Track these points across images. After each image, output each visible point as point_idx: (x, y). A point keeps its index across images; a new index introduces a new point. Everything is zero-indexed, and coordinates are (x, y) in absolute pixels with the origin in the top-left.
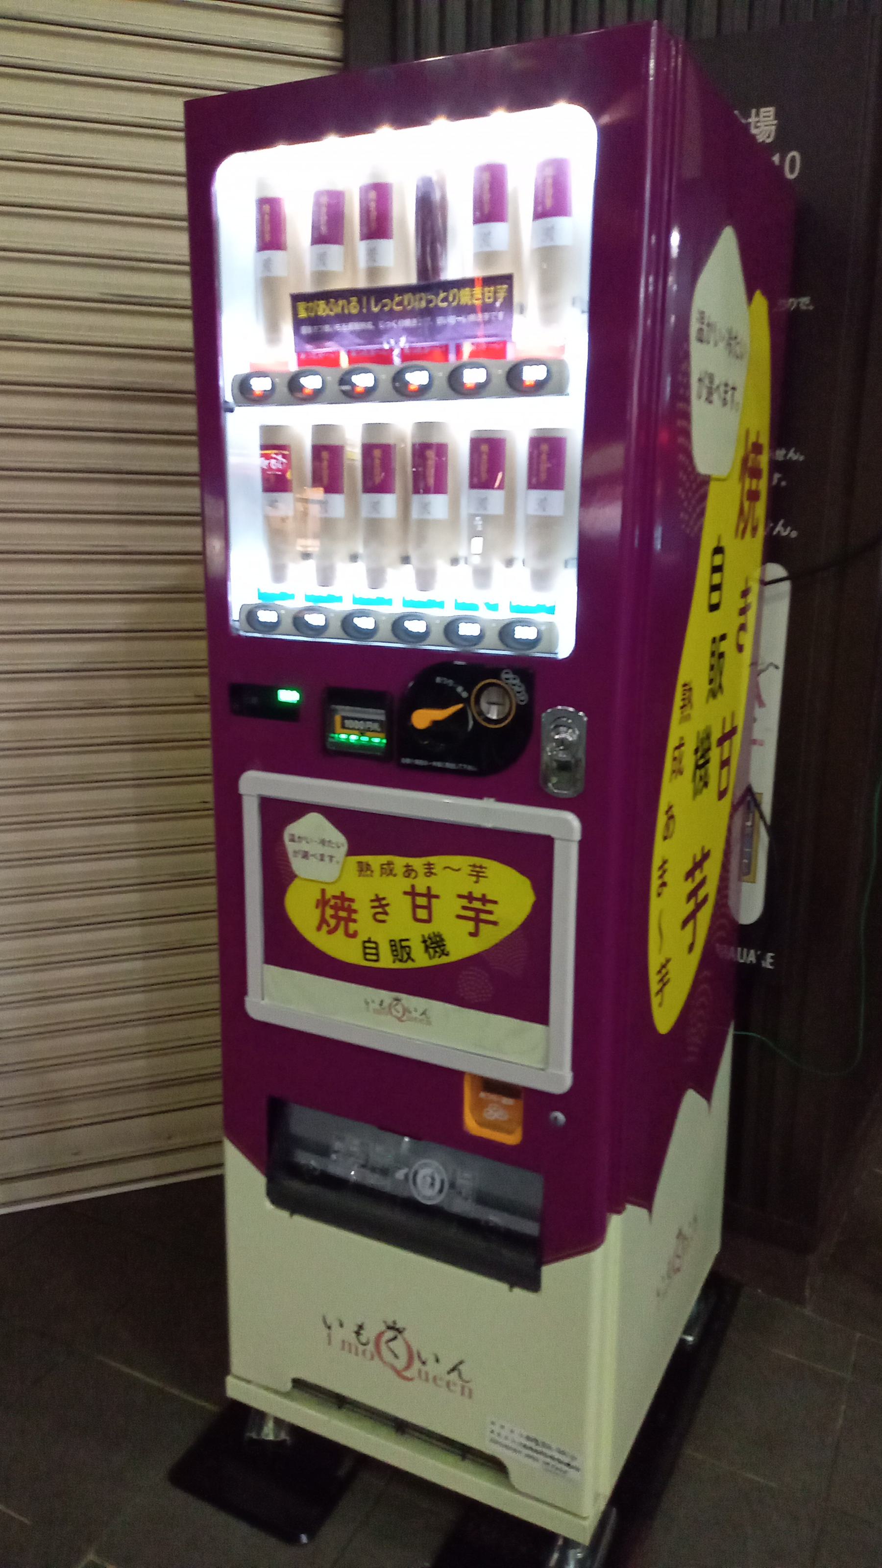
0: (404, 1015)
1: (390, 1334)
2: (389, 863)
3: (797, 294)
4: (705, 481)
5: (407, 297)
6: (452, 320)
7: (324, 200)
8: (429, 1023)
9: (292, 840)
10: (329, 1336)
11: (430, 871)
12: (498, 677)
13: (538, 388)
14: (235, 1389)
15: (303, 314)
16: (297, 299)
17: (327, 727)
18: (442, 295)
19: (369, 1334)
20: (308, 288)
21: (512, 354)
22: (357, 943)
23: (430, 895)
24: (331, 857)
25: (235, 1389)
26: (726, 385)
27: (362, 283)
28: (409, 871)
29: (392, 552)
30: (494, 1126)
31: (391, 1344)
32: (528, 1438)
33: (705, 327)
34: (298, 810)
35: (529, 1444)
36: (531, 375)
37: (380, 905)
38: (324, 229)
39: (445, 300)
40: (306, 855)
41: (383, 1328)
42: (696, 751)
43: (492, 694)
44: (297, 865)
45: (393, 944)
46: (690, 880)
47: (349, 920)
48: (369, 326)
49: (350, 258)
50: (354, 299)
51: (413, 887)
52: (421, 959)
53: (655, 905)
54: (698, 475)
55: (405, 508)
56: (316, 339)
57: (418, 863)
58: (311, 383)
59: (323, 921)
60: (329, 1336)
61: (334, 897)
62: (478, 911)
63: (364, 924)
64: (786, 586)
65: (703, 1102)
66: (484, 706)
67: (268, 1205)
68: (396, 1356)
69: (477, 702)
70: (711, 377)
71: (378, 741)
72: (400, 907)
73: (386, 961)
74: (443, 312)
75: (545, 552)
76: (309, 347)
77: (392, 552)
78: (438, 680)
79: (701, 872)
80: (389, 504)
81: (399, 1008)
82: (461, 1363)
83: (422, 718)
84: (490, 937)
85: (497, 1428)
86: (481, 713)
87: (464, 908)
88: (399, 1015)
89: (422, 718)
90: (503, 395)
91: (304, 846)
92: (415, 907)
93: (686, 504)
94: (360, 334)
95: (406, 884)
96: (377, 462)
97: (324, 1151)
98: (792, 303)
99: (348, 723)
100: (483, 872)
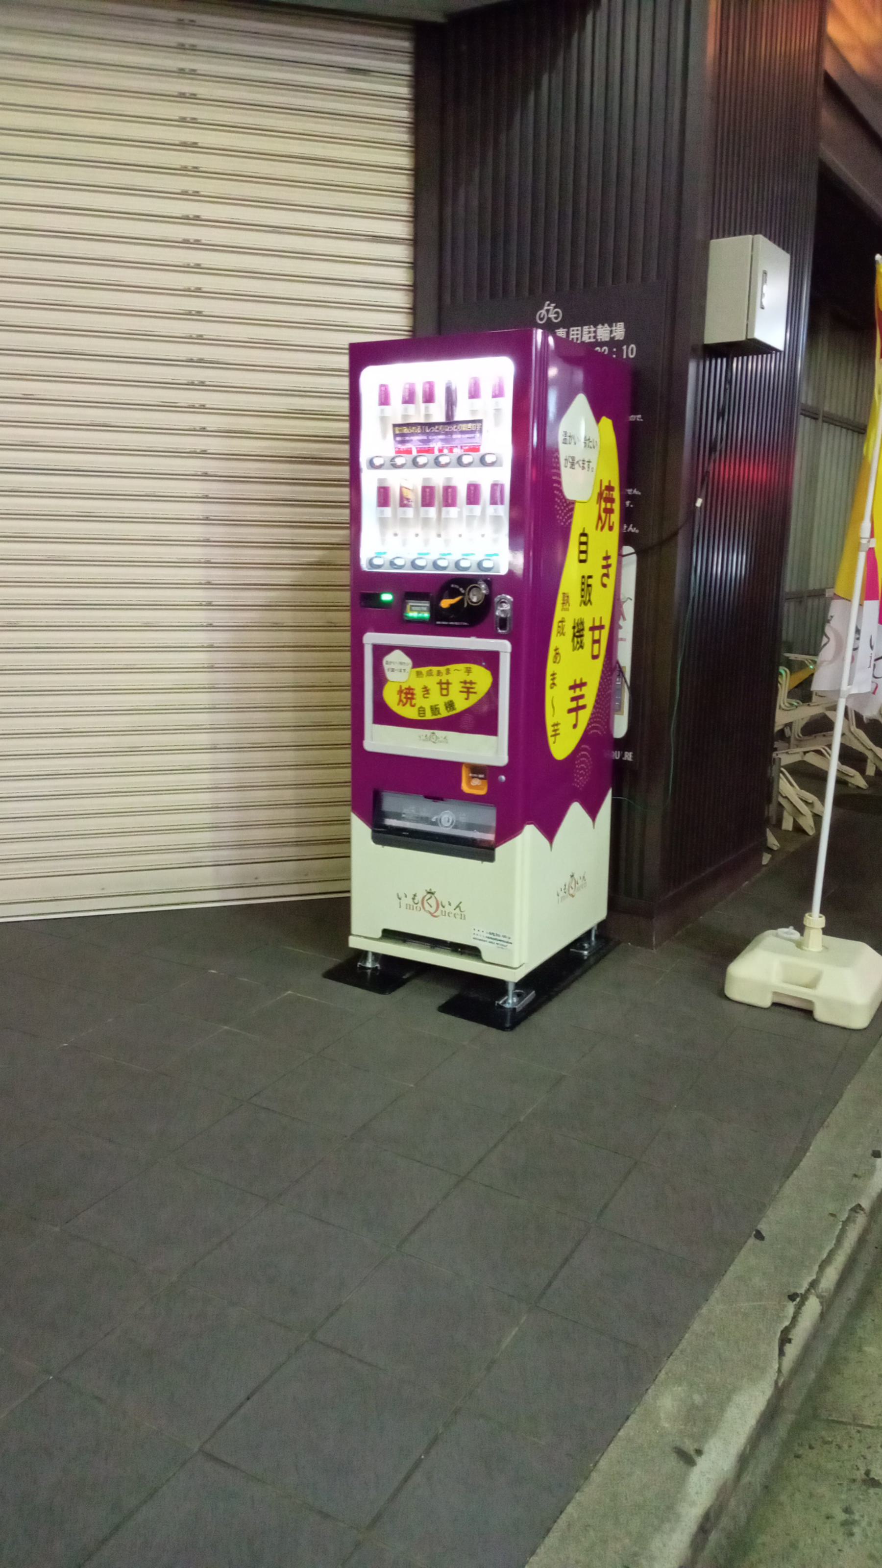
0: (437, 910)
1: (429, 896)
2: (431, 670)
3: (635, 413)
4: (573, 503)
5: (441, 427)
6: (459, 436)
7: (407, 386)
8: (447, 743)
9: (387, 664)
10: (400, 903)
11: (448, 672)
12: (477, 583)
13: (492, 464)
14: (354, 942)
15: (397, 432)
16: (395, 426)
17: (403, 609)
18: (455, 427)
19: (419, 898)
20: (400, 422)
21: (483, 451)
22: (415, 709)
23: (448, 683)
24: (404, 670)
25: (354, 942)
26: (584, 461)
27: (422, 421)
28: (439, 673)
29: (433, 533)
30: (477, 787)
31: (429, 901)
32: (490, 934)
33: (568, 438)
34: (390, 649)
35: (490, 936)
36: (489, 459)
37: (426, 690)
38: (407, 398)
39: (456, 428)
40: (393, 670)
41: (425, 893)
42: (574, 628)
43: (474, 591)
44: (389, 675)
45: (432, 707)
46: (572, 691)
47: (412, 699)
48: (425, 437)
49: (418, 411)
50: (419, 427)
51: (441, 680)
52: (444, 713)
53: (549, 693)
54: (566, 500)
55: (439, 512)
56: (403, 442)
57: (443, 669)
58: (400, 461)
59: (401, 700)
60: (400, 903)
61: (406, 689)
62: (468, 688)
63: (419, 701)
64: (634, 557)
65: (588, 819)
66: (471, 595)
67: (372, 843)
68: (431, 906)
69: (468, 594)
70: (573, 458)
71: (426, 615)
72: (435, 689)
73: (429, 716)
74: (456, 433)
75: (497, 530)
76: (400, 446)
77: (433, 533)
78: (452, 586)
79: (581, 690)
80: (432, 512)
81: (432, 902)
82: (461, 903)
83: (445, 603)
84: (474, 699)
85: (476, 932)
86: (469, 599)
87: (463, 687)
88: (432, 910)
89: (445, 603)
90: (479, 466)
91: (392, 666)
92: (442, 689)
93: (560, 512)
94: (423, 441)
95: (438, 679)
96: (428, 494)
97: (398, 816)
98: (632, 418)
99: (413, 608)
100: (472, 688)
